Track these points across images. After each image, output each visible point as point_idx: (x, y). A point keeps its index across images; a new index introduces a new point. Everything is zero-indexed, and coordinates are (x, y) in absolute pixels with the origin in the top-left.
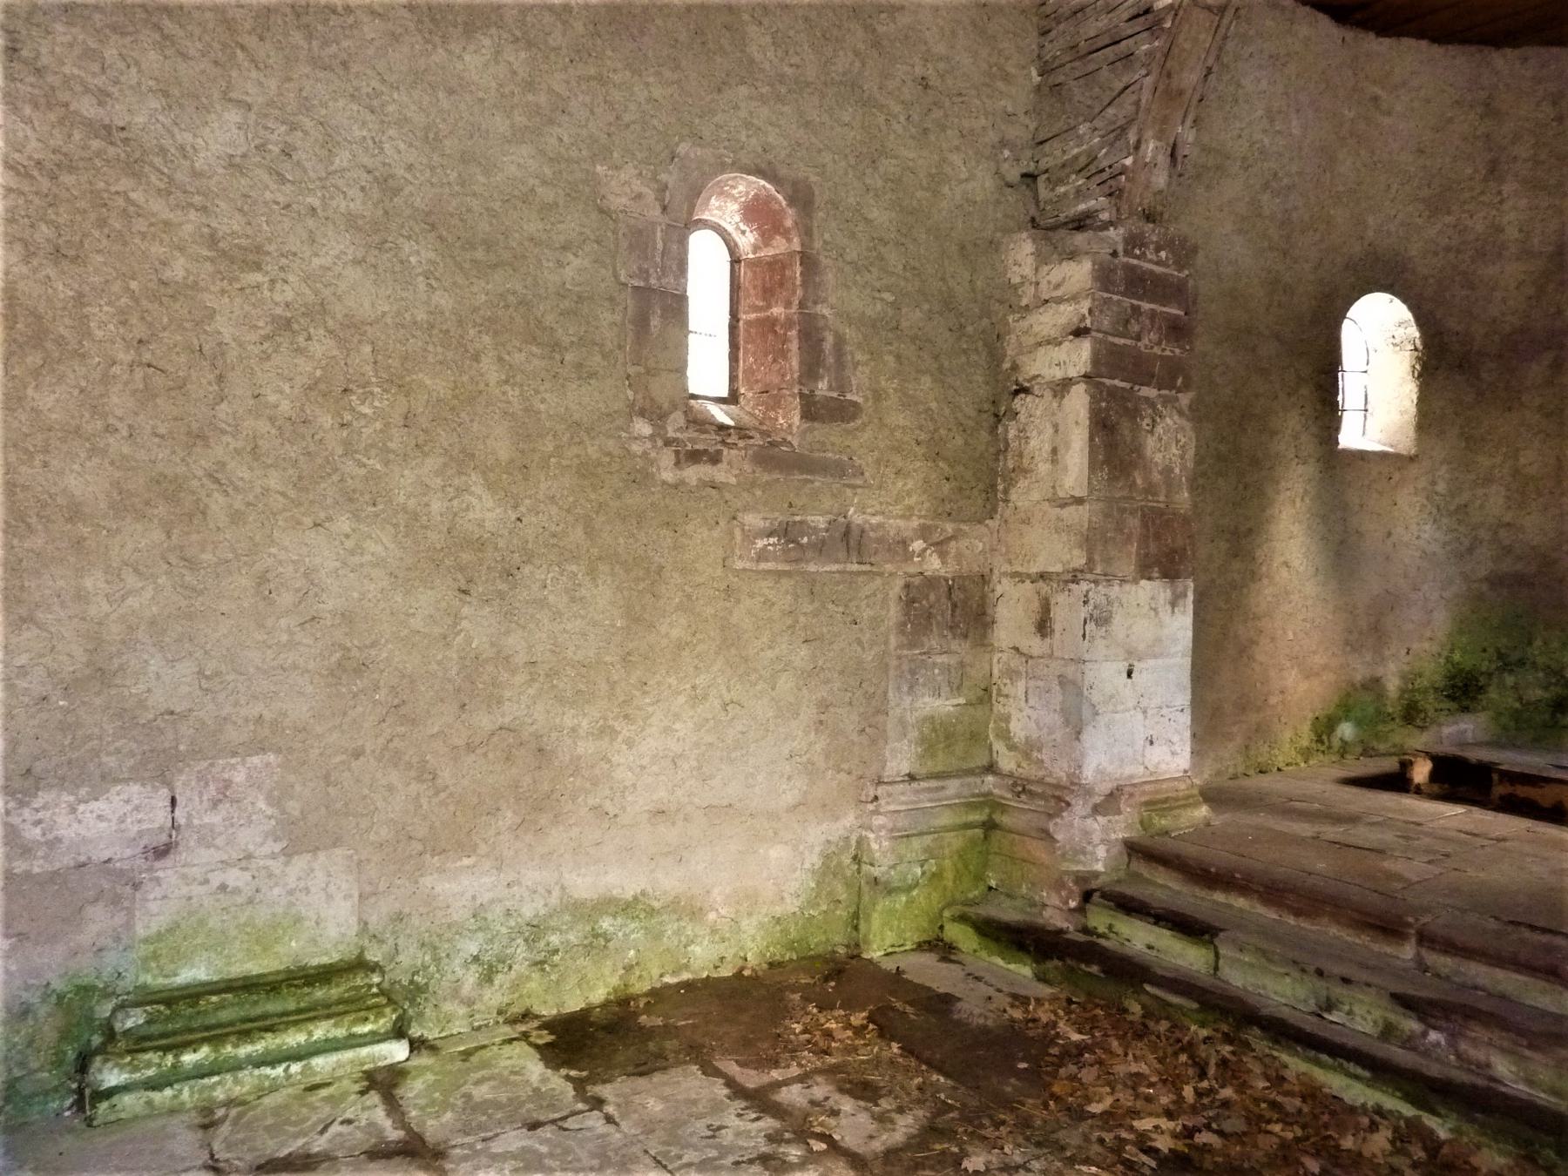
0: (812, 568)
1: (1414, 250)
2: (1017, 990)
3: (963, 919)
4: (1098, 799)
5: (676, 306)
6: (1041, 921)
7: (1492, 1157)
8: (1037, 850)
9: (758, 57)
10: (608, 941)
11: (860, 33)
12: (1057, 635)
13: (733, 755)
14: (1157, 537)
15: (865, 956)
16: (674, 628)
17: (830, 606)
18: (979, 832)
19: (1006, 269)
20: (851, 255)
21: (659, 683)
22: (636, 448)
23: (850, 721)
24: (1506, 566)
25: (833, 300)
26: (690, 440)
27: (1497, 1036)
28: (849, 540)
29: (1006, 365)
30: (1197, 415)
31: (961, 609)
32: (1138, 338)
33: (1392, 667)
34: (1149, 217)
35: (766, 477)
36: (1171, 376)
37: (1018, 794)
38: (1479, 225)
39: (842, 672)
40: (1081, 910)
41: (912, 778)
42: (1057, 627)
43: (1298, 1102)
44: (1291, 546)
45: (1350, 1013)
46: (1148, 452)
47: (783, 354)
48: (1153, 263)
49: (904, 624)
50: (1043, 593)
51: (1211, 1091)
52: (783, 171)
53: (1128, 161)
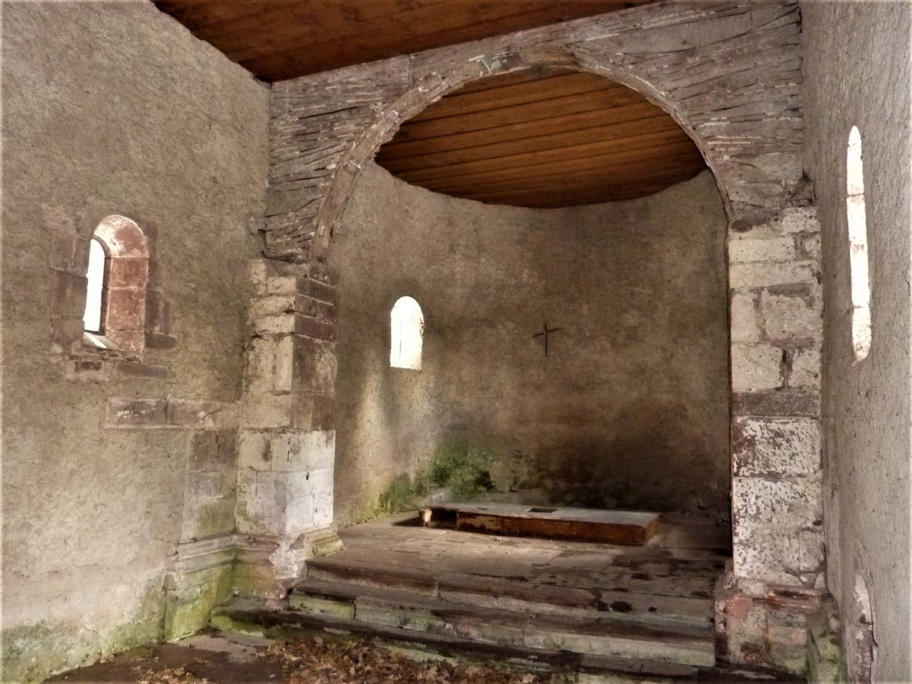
0: (147, 427)
1: (421, 279)
2: (256, 644)
3: (223, 613)
4: (292, 542)
5: (82, 284)
6: (264, 608)
7: (473, 669)
8: (262, 571)
9: (133, 157)
10: (19, 654)
11: (186, 152)
12: (274, 460)
13: (99, 534)
14: (321, 410)
15: (169, 642)
16: (69, 463)
17: (155, 448)
18: (229, 566)
19: (250, 276)
20: (175, 263)
21: (58, 496)
22: (53, 360)
23: (163, 510)
24: (458, 421)
25: (164, 284)
26: (84, 356)
27: (471, 620)
28: (167, 412)
29: (249, 323)
30: (337, 351)
31: (223, 447)
32: (315, 315)
33: (412, 468)
34: (320, 260)
35: (125, 378)
36: (328, 334)
37: (251, 543)
38: (446, 271)
39: (160, 484)
40: (286, 599)
41: (195, 540)
42: (274, 455)
43: (397, 665)
44: (371, 413)
45: (414, 623)
47: (135, 310)
48: (322, 281)
49: (194, 456)
50: (267, 438)
51: (361, 668)
52: (143, 217)
53: (313, 234)
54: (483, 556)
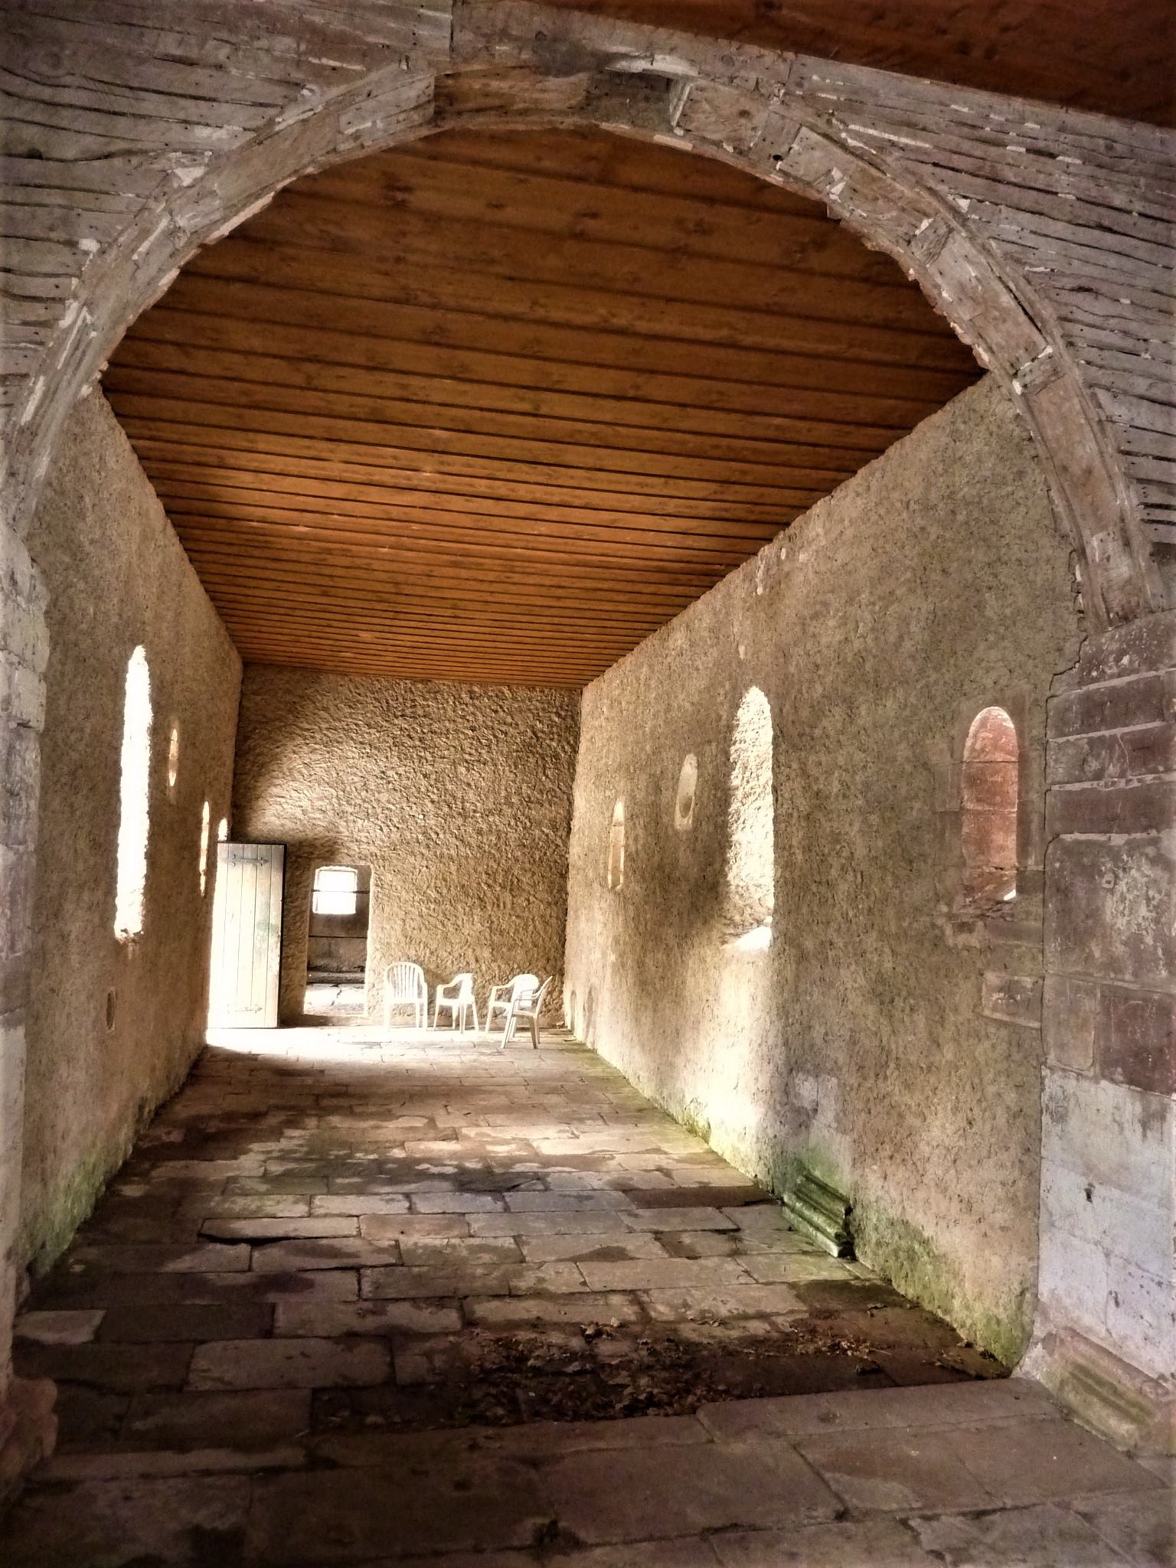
14: (1121, 1027)
46: (1108, 918)
54: (439, 1074)
